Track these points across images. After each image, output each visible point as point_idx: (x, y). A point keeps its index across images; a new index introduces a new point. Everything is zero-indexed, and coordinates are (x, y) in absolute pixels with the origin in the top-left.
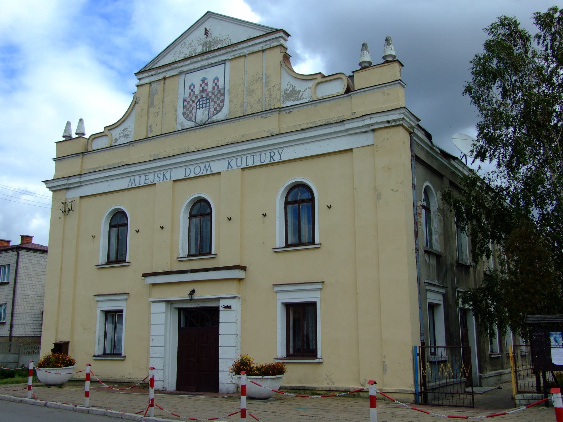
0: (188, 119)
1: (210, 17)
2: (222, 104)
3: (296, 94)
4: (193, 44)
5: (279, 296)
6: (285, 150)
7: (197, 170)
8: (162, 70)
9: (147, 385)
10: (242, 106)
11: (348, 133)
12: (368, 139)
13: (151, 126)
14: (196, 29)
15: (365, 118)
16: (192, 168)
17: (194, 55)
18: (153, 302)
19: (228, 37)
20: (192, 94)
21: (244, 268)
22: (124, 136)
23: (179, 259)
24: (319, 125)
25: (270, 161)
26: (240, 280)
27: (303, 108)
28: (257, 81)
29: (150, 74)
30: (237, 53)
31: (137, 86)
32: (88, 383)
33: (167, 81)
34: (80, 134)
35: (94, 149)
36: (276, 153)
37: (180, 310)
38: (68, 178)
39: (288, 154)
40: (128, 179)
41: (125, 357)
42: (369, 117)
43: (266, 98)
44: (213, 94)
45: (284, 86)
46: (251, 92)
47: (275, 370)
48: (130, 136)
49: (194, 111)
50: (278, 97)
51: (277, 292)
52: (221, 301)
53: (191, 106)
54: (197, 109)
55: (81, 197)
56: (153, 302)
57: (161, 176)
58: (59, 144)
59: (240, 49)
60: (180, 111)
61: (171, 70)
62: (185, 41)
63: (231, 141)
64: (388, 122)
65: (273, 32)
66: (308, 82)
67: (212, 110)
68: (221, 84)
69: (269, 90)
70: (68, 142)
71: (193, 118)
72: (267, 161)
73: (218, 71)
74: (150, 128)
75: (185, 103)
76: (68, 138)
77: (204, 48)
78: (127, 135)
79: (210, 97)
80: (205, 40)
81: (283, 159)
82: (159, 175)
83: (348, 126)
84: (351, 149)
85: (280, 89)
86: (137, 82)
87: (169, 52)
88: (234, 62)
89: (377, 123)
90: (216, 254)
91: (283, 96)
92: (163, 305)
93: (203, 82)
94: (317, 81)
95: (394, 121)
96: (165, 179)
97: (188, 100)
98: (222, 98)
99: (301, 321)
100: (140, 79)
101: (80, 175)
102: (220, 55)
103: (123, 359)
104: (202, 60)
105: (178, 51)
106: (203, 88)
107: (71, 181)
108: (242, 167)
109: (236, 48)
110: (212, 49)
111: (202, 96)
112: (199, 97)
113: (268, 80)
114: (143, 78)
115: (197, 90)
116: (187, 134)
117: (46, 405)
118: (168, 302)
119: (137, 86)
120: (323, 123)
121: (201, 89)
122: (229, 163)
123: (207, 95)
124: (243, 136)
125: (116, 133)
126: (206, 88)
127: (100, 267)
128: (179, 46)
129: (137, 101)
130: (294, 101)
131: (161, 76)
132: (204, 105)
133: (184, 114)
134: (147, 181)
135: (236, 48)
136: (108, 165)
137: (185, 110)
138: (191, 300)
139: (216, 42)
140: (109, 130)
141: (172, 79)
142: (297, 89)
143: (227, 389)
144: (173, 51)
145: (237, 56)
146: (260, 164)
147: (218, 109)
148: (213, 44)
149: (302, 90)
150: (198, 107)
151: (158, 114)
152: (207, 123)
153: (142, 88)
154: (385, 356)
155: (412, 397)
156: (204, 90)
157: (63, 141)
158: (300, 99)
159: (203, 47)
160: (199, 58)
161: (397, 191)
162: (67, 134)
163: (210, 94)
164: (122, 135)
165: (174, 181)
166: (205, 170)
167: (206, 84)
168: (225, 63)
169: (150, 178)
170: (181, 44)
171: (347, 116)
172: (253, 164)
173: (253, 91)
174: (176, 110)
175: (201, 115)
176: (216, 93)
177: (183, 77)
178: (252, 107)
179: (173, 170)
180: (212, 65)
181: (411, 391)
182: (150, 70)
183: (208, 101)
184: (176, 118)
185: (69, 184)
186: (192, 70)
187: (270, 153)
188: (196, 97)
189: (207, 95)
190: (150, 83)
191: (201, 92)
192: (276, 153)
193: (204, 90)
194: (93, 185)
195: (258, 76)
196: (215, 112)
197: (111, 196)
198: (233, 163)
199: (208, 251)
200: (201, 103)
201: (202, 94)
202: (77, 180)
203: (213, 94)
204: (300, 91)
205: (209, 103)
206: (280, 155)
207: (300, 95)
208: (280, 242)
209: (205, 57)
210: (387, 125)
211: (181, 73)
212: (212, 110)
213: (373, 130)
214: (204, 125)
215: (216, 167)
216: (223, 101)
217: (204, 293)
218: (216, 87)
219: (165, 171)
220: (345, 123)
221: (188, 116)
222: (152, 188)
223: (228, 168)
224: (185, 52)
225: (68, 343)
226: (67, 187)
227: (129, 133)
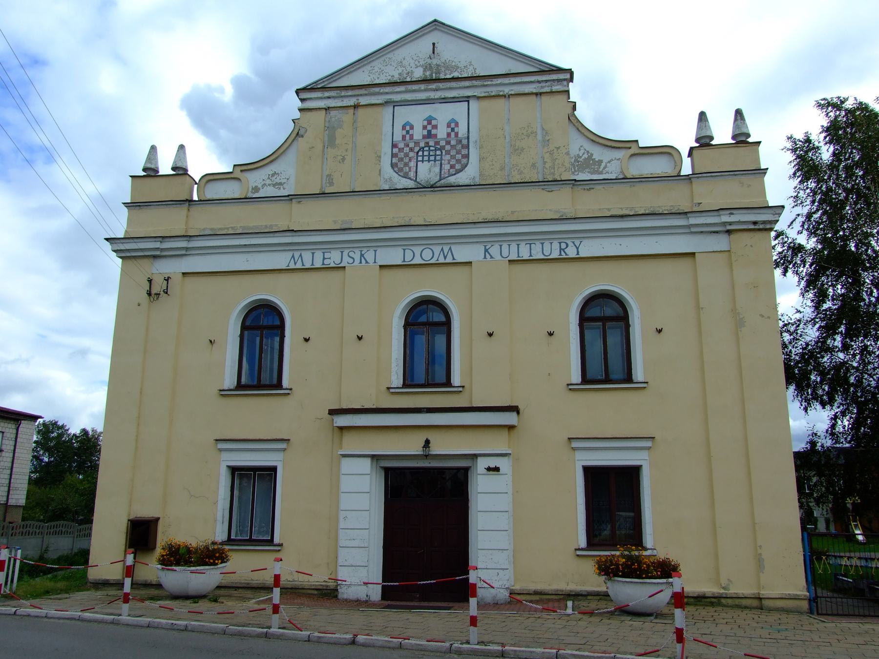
0: (401, 174)
1: (436, 29)
2: (464, 161)
3: (594, 164)
4: (405, 63)
5: (579, 455)
6: (585, 242)
7: (427, 255)
8: (350, 93)
9: (328, 594)
10: (502, 169)
11: (690, 230)
12: (721, 243)
13: (329, 176)
14: (411, 41)
15: (721, 212)
16: (417, 250)
17: (408, 79)
18: (344, 456)
19: (471, 64)
20: (408, 137)
21: (515, 409)
22: (274, 185)
23: (571, 387)
24: (640, 213)
25: (560, 255)
26: (511, 428)
27: (611, 185)
28: (528, 136)
29: (327, 94)
30: (494, 91)
31: (300, 110)
32: (277, 591)
33: (360, 111)
34: (180, 171)
35: (209, 197)
36: (570, 244)
37: (387, 470)
38: (731, 210)
39: (589, 248)
40: (290, 254)
41: (281, 545)
42: (729, 212)
43: (545, 163)
44: (448, 143)
45: (574, 150)
46: (517, 151)
47: (210, 556)
48: (285, 186)
49: (412, 164)
50: (567, 165)
51: (221, 450)
52: (480, 459)
53: (406, 155)
54: (417, 161)
55: (183, 274)
56: (344, 456)
57: (357, 257)
58: (138, 180)
59: (496, 85)
60: (386, 160)
61: (366, 95)
62: (389, 56)
63: (490, 217)
64: (755, 223)
65: (552, 70)
66: (613, 150)
67: (447, 167)
68: (462, 131)
69: (551, 153)
70: (177, 178)
71: (412, 174)
72: (555, 255)
73: (458, 111)
74: (330, 180)
75: (395, 150)
76: (151, 172)
77: (428, 73)
78: (281, 184)
79: (443, 148)
80: (429, 61)
81: (582, 255)
82: (351, 254)
83: (693, 221)
84: (694, 254)
85: (568, 154)
86: (299, 104)
87: (359, 68)
88: (486, 103)
89: (739, 222)
90: (463, 387)
91: (573, 165)
92: (368, 461)
93: (429, 123)
94: (631, 151)
95: (764, 222)
96: (363, 260)
97: (401, 145)
98: (464, 152)
99: (613, 496)
100: (302, 100)
101: (189, 237)
102: (460, 88)
103: (279, 548)
104: (426, 90)
105: (376, 69)
106: (429, 132)
107: (166, 245)
108: (509, 258)
109: (489, 83)
110: (442, 76)
111: (428, 143)
112: (422, 144)
113: (547, 138)
114: (310, 99)
115: (418, 133)
116: (395, 199)
117: (353, 642)
118: (373, 457)
119: (300, 110)
120: (647, 212)
121: (425, 132)
122: (486, 251)
123: (437, 143)
124: (513, 212)
125: (255, 179)
126: (434, 132)
127: (224, 393)
128: (378, 61)
129: (301, 133)
130: (592, 174)
131: (352, 102)
132: (432, 158)
133: (393, 166)
134: (326, 262)
135: (489, 83)
136: (243, 228)
137: (394, 160)
138: (426, 456)
139: (448, 67)
140: (242, 171)
141: (370, 110)
142: (596, 157)
143: (494, 597)
144: (368, 68)
145: (493, 94)
146: (542, 257)
147: (458, 167)
148: (443, 69)
149: (605, 161)
150: (420, 158)
151: (343, 159)
152: (438, 184)
153: (309, 114)
154: (760, 547)
155: (805, 605)
156: (429, 135)
157: (144, 176)
158: (601, 173)
159: (424, 71)
160: (423, 87)
161: (769, 317)
162: (149, 166)
163: (443, 143)
164: (268, 182)
165: (380, 266)
166: (442, 256)
167: (435, 127)
168: (468, 101)
169: (334, 258)
170: (383, 58)
171: (685, 207)
172: (531, 256)
173: (522, 149)
174: (380, 157)
175: (426, 171)
176: (453, 142)
177: (390, 109)
178: (521, 173)
179: (379, 250)
180: (445, 100)
181: (805, 596)
182: (324, 88)
183: (438, 153)
184: (380, 171)
185: (162, 250)
186: (409, 101)
187: (560, 243)
188: (417, 143)
189: (437, 143)
190: (327, 109)
191: (424, 137)
192: (570, 244)
193: (429, 135)
194: (213, 256)
195: (530, 130)
196: (452, 171)
197: (624, 264)
198: (494, 250)
199: (444, 380)
200: (426, 153)
201: (427, 140)
202: (183, 244)
203: (448, 143)
204: (601, 162)
205: (441, 155)
206: (577, 248)
207: (602, 167)
208: (230, 381)
209: (434, 86)
210: (752, 227)
211: (387, 103)
212: (447, 167)
213: (729, 232)
214: (432, 187)
215: (462, 253)
216: (467, 156)
217: (447, 446)
218: (453, 134)
219: (365, 250)
220: (689, 215)
221: (401, 170)
222: (338, 274)
223: (485, 258)
224: (392, 73)
225: (158, 519)
226: (158, 253)
227: (283, 181)
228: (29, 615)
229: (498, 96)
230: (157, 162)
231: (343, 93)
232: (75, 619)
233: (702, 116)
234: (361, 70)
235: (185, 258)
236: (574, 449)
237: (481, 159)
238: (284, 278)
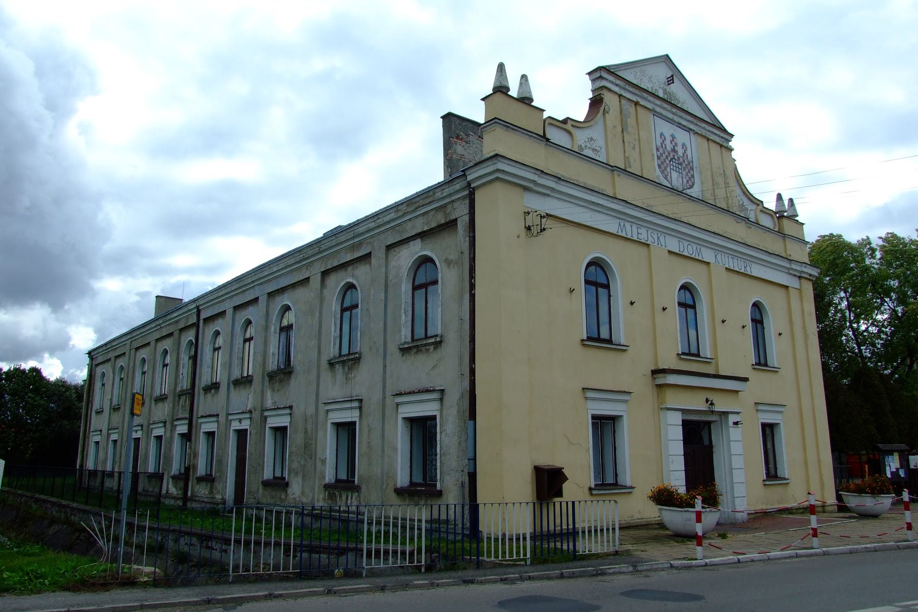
11: (789, 272)
169: (644, 236)
175: (676, 180)
215: (707, 255)
226: (532, 186)
228: (753, 561)
229: (705, 137)
230: (530, 92)
231: (627, 87)
232: (793, 557)
233: (501, 67)
234: (631, 70)
235: (547, 199)
236: (757, 410)
237: (702, 183)
238: (611, 241)
